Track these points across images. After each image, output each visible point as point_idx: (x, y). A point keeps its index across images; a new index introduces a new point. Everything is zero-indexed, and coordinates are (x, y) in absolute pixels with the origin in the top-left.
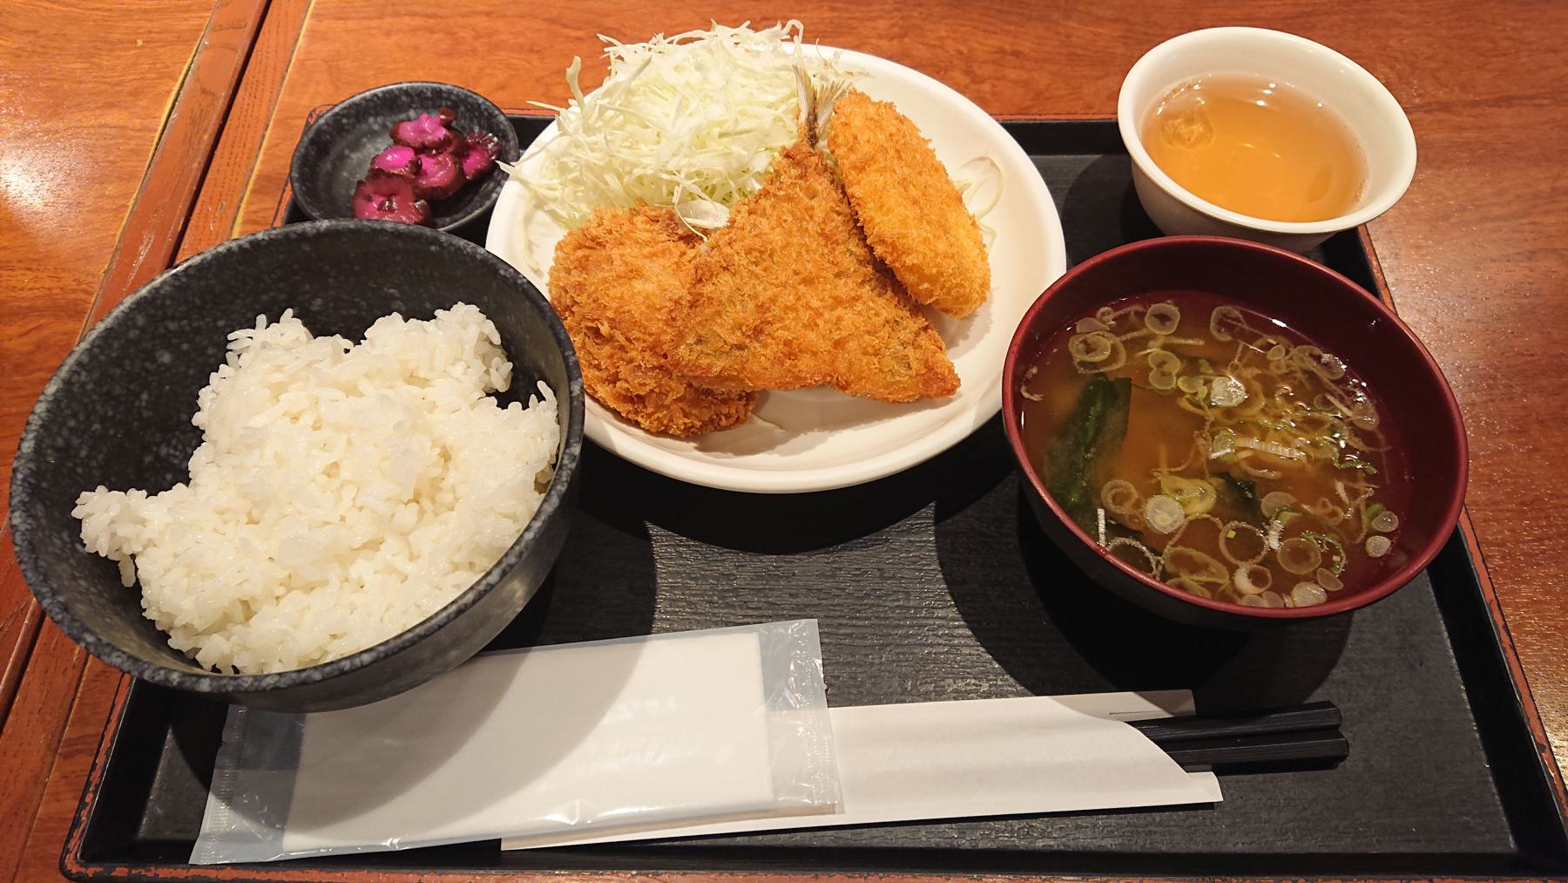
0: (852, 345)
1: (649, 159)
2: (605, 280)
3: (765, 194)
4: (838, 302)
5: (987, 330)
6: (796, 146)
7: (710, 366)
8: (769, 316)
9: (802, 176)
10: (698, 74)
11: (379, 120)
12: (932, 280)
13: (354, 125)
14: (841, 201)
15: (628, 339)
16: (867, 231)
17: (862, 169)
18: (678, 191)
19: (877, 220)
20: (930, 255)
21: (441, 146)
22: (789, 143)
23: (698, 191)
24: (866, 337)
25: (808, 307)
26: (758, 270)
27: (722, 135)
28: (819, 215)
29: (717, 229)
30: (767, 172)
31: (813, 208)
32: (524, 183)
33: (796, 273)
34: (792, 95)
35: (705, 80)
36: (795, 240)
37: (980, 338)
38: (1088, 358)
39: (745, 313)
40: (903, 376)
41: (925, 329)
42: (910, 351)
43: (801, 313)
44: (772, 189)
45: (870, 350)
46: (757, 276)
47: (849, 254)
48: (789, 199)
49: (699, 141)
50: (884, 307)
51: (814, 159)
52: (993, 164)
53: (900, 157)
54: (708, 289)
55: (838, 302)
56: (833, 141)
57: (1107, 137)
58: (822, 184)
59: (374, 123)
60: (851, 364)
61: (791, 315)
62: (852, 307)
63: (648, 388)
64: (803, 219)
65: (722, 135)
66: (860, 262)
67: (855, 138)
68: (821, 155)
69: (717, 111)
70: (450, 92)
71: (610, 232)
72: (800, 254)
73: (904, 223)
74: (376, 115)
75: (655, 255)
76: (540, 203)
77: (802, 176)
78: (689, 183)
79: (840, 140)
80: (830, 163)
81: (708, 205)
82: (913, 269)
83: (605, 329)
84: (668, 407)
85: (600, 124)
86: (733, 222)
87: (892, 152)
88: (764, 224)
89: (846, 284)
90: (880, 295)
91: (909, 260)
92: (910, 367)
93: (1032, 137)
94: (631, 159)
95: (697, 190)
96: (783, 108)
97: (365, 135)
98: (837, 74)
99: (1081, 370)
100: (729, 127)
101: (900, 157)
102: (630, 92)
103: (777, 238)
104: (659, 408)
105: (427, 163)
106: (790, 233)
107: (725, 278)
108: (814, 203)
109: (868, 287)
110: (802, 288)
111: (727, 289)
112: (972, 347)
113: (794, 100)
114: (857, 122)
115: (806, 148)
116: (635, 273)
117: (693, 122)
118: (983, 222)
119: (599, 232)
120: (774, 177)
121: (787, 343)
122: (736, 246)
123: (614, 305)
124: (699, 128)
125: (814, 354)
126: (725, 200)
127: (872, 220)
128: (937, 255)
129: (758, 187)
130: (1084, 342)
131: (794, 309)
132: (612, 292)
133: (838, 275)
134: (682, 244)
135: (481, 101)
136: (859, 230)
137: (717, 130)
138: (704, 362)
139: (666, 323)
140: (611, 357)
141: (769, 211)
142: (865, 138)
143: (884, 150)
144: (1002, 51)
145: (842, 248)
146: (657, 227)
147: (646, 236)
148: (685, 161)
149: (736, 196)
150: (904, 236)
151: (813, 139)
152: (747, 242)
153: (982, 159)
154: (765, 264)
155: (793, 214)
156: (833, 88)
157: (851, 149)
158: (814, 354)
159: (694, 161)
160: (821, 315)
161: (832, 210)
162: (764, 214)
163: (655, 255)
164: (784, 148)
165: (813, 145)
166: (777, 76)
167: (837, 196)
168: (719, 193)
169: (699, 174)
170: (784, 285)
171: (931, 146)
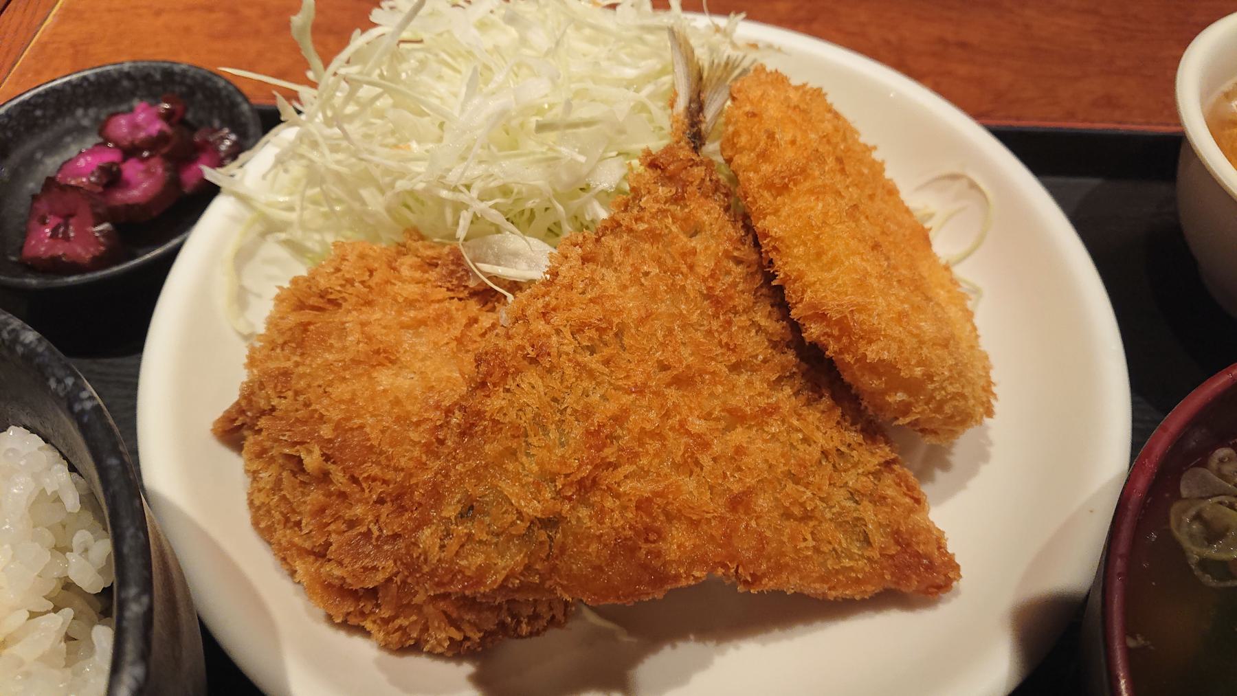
0: (763, 502)
1: (420, 164)
2: (328, 366)
3: (613, 226)
4: (736, 417)
5: (984, 457)
6: (668, 150)
7: (482, 572)
8: (609, 453)
9: (677, 199)
10: (513, 32)
11: (92, 112)
12: (913, 386)
13: (53, 119)
14: (742, 241)
15: (354, 480)
16: (790, 295)
17: (781, 189)
18: (465, 219)
19: (811, 277)
20: (911, 343)
21: (155, 144)
22: (656, 145)
23: (499, 219)
24: (790, 487)
25: (682, 429)
26: (592, 361)
27: (541, 128)
28: (705, 264)
29: (531, 282)
30: (619, 191)
31: (694, 252)
32: (243, 199)
33: (664, 367)
34: (663, 72)
35: (523, 41)
36: (663, 308)
37: (972, 472)
38: (1213, 552)
39: (561, 449)
40: (856, 560)
41: (888, 464)
42: (868, 512)
43: (670, 443)
44: (626, 219)
45: (796, 511)
46: (591, 374)
47: (755, 330)
48: (654, 236)
49: (507, 133)
50: (819, 428)
51: (699, 171)
52: (973, 186)
53: (843, 171)
54: (496, 403)
55: (736, 417)
56: (730, 144)
57: (1170, 150)
58: (710, 213)
59: (85, 117)
60: (762, 538)
61: (653, 446)
62: (761, 426)
63: (381, 577)
64: (676, 271)
65: (541, 128)
66: (774, 345)
67: (771, 136)
68: (709, 164)
69: (538, 90)
70: (184, 74)
71: (350, 282)
72: (670, 331)
73: (861, 284)
74: (87, 106)
75: (422, 323)
76: (270, 227)
77: (677, 199)
78: (484, 205)
79: (743, 140)
80: (723, 179)
81: (515, 241)
82: (875, 369)
83: (312, 460)
84: (419, 608)
85: (351, 109)
86: (554, 274)
87: (831, 162)
88: (609, 280)
89: (749, 383)
90: (809, 403)
91: (872, 353)
92: (867, 541)
93: (1040, 151)
94: (392, 164)
95: (497, 217)
96: (649, 89)
97: (68, 132)
98: (734, 45)
99: (1208, 579)
100: (556, 114)
101: (843, 171)
102: (396, 57)
103: (631, 304)
104: (402, 608)
105: (132, 170)
106: (654, 295)
107: (531, 377)
108: (695, 243)
109: (788, 391)
110: (673, 394)
111: (532, 401)
112: (960, 485)
113: (667, 79)
114: (772, 111)
115: (685, 153)
116: (383, 356)
117: (494, 105)
118: (959, 271)
119: (335, 283)
120: (629, 200)
121: (643, 505)
122: (557, 319)
123: (335, 415)
124: (503, 113)
125: (694, 524)
126: (552, 233)
127: (800, 277)
128: (921, 343)
129: (603, 214)
130: (1198, 517)
131: (657, 435)
132: (340, 390)
133: (735, 368)
134: (474, 306)
135: (222, 84)
136: (776, 295)
137: (533, 121)
138: (474, 561)
139: (428, 449)
140: (322, 510)
141: (618, 257)
142: (789, 137)
143: (819, 158)
144: (942, 41)
145: (743, 319)
146: (433, 275)
147: (412, 290)
148: (479, 170)
149: (568, 229)
150: (862, 309)
151: (697, 139)
152: (577, 312)
153: (954, 177)
154: (607, 352)
155: (659, 261)
156: (729, 66)
157: (764, 156)
158: (694, 524)
159: (495, 170)
160: (706, 446)
161: (727, 254)
162: (609, 262)
163: (422, 323)
164: (648, 153)
165: (696, 149)
166: (641, 40)
167: (735, 232)
168: (542, 222)
169: (505, 191)
170: (640, 391)
171: (877, 156)
